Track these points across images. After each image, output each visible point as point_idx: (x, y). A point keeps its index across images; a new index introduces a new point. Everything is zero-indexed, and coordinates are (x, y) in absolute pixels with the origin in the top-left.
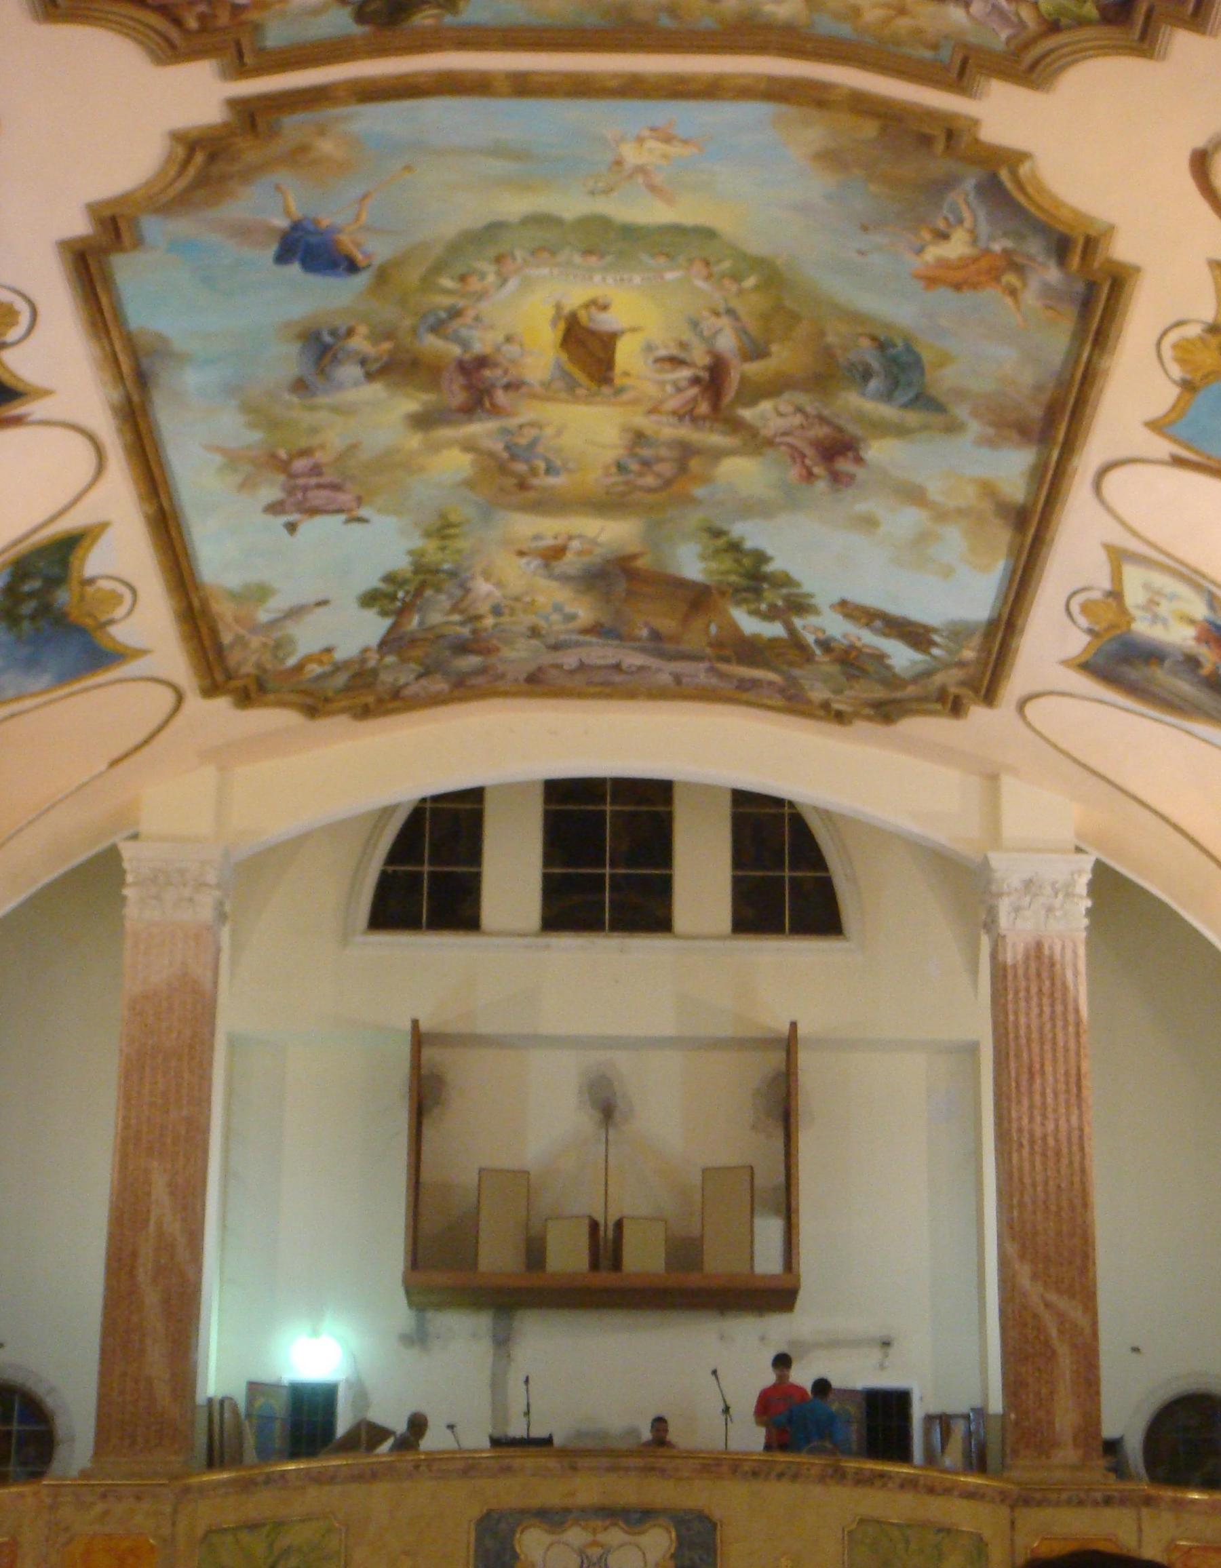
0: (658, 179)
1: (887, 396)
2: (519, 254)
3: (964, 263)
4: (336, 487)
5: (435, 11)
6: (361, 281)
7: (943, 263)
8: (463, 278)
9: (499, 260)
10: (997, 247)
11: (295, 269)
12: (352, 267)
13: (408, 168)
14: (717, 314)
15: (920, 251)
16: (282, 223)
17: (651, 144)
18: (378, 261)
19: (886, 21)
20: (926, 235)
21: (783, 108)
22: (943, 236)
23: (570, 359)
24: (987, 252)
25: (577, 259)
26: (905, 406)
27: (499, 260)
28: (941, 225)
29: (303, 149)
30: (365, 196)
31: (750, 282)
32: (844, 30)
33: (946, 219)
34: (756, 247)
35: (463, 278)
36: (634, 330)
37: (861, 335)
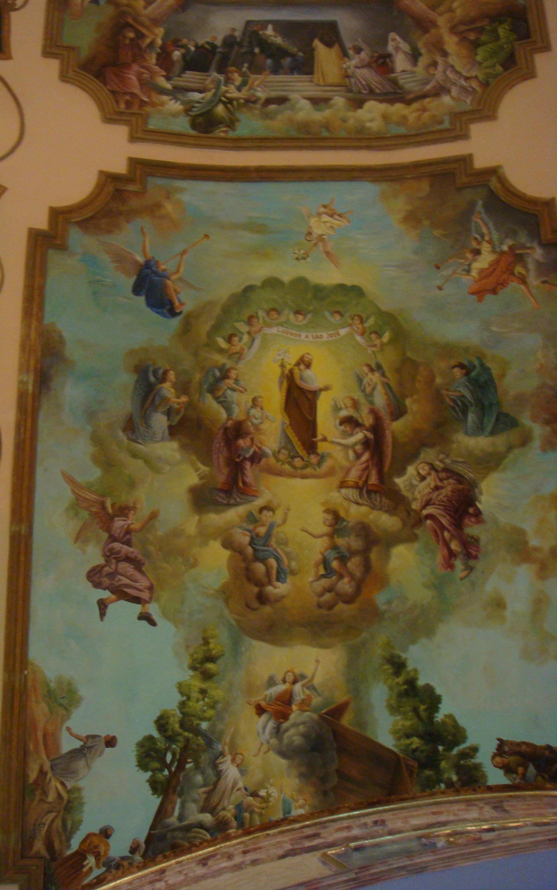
0: (330, 246)
1: (479, 429)
2: (261, 314)
3: (494, 264)
4: (137, 564)
5: (224, 129)
6: (175, 323)
7: (484, 274)
8: (229, 339)
9: (250, 321)
10: (505, 248)
11: (141, 300)
12: (173, 313)
13: (206, 236)
14: (372, 370)
15: (468, 271)
16: (141, 259)
17: (325, 218)
18: (186, 309)
19: (419, 118)
20: (469, 256)
21: (384, 186)
22: (477, 252)
23: (291, 424)
24: (502, 253)
25: (292, 317)
26: (493, 433)
27: (250, 321)
28: (474, 245)
29: (158, 206)
30: (184, 252)
31: (386, 337)
32: (402, 130)
33: (476, 239)
34: (386, 305)
35: (229, 339)
36: (326, 389)
37: (455, 367)
